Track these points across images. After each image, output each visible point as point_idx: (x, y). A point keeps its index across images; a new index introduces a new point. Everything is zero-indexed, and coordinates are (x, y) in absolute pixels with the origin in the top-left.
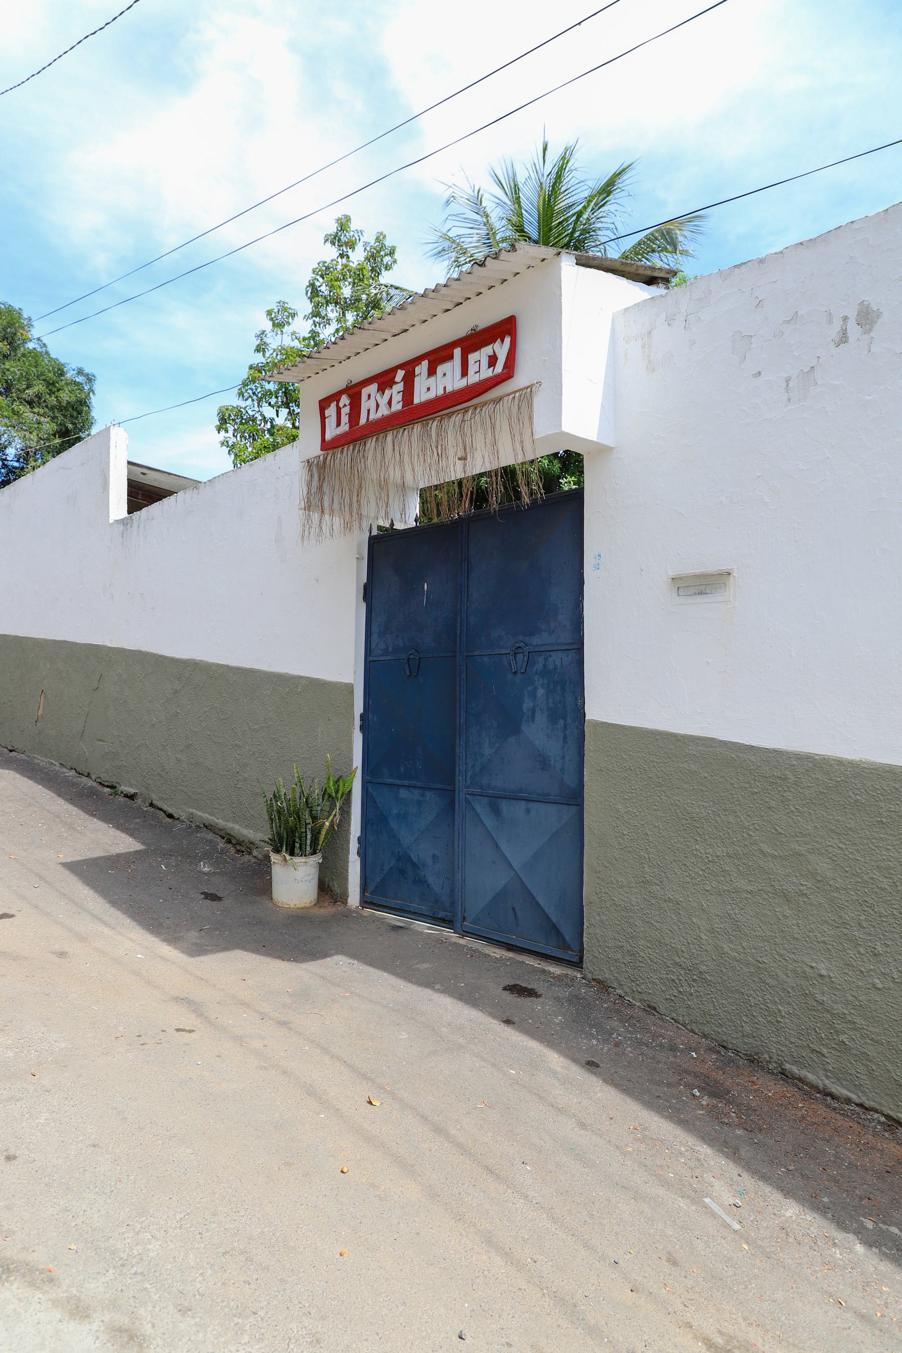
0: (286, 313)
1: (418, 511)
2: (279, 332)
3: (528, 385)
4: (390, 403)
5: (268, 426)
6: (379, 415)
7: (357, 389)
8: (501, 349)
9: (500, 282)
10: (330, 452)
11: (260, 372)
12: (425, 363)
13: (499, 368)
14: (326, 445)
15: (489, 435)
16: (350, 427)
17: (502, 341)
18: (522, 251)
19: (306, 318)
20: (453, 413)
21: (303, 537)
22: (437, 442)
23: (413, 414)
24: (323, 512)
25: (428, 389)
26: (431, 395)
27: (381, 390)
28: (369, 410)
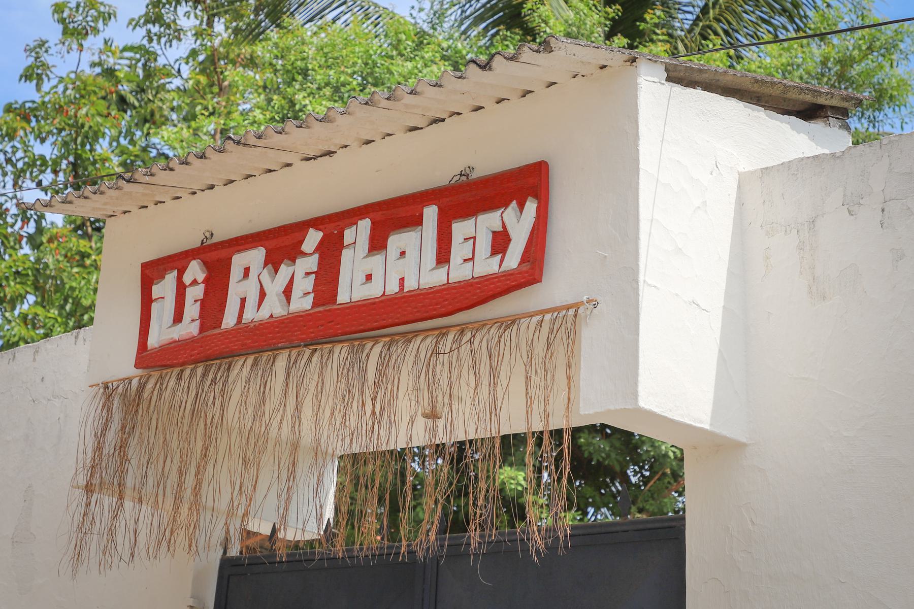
0: (93, 12)
1: (329, 513)
2: (75, 46)
3: (570, 300)
4: (288, 292)
5: (31, 228)
6: (264, 314)
7: (223, 253)
8: (519, 222)
9: (520, 94)
10: (156, 374)
11: (26, 119)
12: (365, 225)
13: (513, 259)
14: (147, 358)
15: (484, 389)
16: (202, 329)
17: (521, 206)
18: (562, 53)
19: (134, 24)
20: (417, 333)
21: (78, 556)
22: (377, 385)
23: (331, 324)
24: (121, 497)
25: (369, 277)
26: (374, 291)
27: (273, 262)
28: (243, 301)
